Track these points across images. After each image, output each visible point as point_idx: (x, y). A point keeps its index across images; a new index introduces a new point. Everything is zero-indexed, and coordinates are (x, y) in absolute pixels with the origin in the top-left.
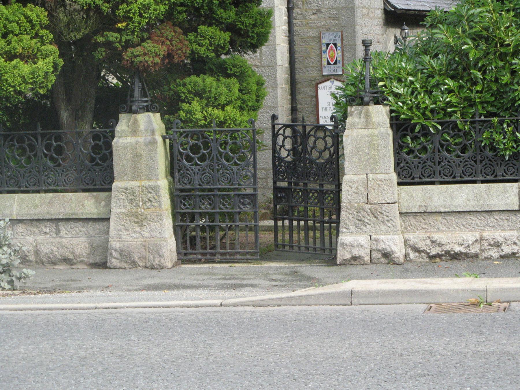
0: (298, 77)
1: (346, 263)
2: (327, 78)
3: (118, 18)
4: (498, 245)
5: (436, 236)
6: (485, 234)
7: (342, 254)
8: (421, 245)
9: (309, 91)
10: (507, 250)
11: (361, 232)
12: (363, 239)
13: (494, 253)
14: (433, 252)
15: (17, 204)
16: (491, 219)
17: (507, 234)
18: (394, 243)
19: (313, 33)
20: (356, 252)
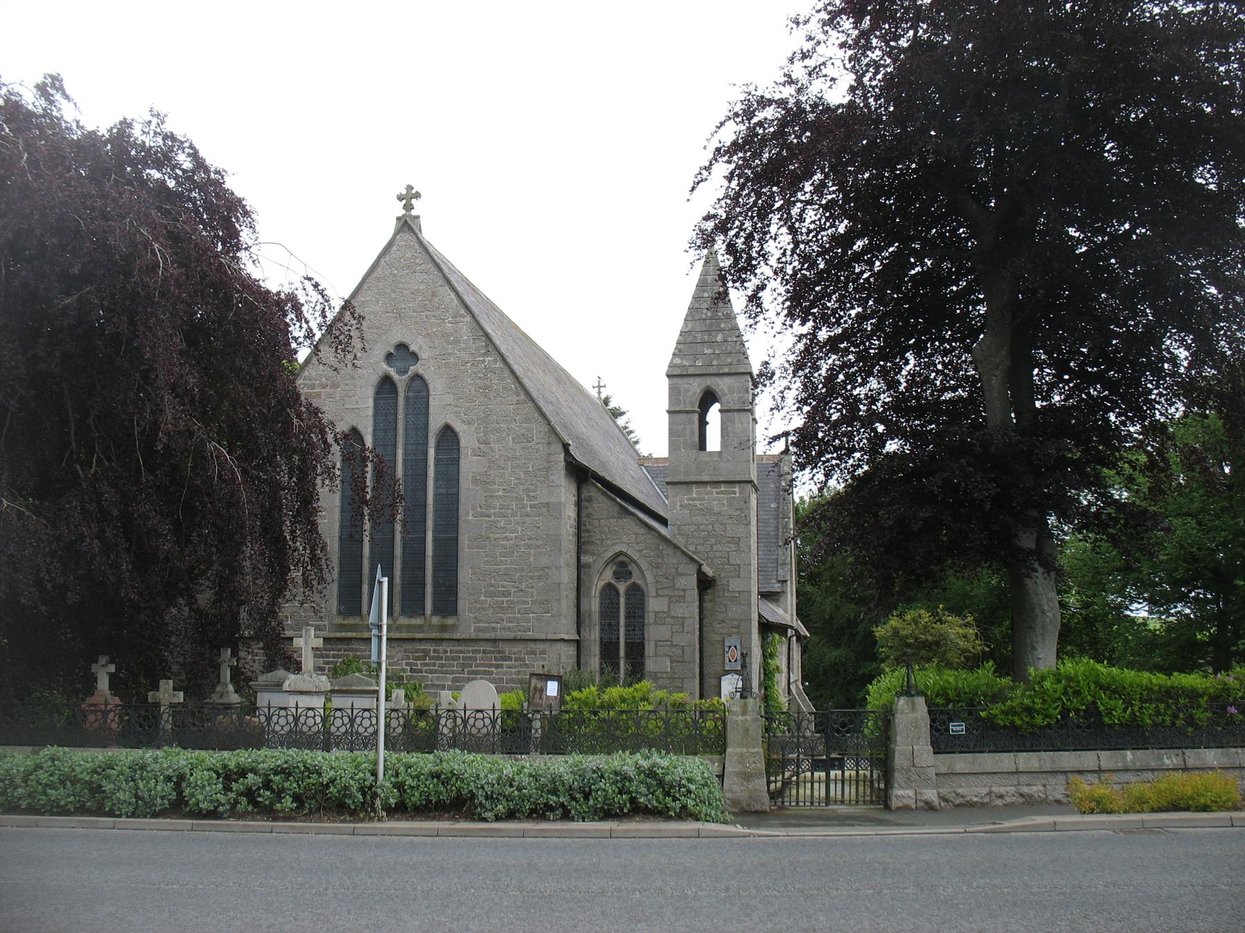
0: (705, 671)
1: (899, 809)
2: (728, 672)
3: (1093, 509)
4: (1001, 797)
5: (960, 791)
6: (994, 789)
7: (894, 803)
8: (949, 796)
9: (714, 682)
10: (1008, 800)
11: (909, 788)
12: (910, 793)
13: (999, 802)
14: (957, 802)
15: (18, 759)
16: (996, 777)
17: (1008, 789)
18: (931, 795)
19: (718, 638)
20: (906, 801)
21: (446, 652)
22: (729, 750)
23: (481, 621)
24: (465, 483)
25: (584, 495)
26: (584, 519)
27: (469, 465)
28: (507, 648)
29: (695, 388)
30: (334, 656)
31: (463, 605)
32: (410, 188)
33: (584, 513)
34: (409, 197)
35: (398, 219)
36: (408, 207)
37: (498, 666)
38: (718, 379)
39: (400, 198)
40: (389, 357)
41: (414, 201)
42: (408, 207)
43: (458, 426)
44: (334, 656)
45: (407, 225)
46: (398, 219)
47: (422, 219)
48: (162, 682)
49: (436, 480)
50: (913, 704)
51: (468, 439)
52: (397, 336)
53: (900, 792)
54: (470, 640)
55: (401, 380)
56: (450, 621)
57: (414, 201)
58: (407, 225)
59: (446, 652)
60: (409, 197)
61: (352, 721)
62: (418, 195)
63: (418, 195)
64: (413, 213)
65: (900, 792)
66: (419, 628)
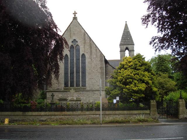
12: (182, 116)
21: (84, 93)
22: (151, 109)
23: (90, 87)
24: (87, 63)
25: (106, 65)
26: (106, 70)
27: (87, 60)
28: (95, 92)
29: (125, 47)
30: (64, 94)
31: (87, 85)
32: (75, 12)
33: (106, 68)
34: (75, 13)
35: (73, 17)
36: (75, 15)
37: (94, 95)
38: (129, 46)
39: (73, 14)
40: (72, 42)
41: (76, 14)
42: (75, 15)
43: (86, 54)
44: (64, 94)
45: (75, 18)
46: (73, 17)
47: (77, 18)
48: (117, 97)
49: (82, 63)
50: (154, 101)
51: (87, 56)
52: (74, 38)
53: (181, 116)
54: (89, 91)
55: (74, 46)
56: (85, 88)
57: (76, 14)
58: (75, 18)
59: (84, 93)
60: (75, 13)
61: (77, 106)
62: (77, 13)
63: (77, 13)
64: (76, 16)
65: (181, 116)
66: (79, 89)
